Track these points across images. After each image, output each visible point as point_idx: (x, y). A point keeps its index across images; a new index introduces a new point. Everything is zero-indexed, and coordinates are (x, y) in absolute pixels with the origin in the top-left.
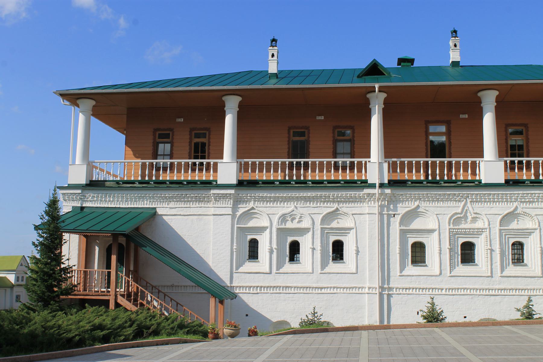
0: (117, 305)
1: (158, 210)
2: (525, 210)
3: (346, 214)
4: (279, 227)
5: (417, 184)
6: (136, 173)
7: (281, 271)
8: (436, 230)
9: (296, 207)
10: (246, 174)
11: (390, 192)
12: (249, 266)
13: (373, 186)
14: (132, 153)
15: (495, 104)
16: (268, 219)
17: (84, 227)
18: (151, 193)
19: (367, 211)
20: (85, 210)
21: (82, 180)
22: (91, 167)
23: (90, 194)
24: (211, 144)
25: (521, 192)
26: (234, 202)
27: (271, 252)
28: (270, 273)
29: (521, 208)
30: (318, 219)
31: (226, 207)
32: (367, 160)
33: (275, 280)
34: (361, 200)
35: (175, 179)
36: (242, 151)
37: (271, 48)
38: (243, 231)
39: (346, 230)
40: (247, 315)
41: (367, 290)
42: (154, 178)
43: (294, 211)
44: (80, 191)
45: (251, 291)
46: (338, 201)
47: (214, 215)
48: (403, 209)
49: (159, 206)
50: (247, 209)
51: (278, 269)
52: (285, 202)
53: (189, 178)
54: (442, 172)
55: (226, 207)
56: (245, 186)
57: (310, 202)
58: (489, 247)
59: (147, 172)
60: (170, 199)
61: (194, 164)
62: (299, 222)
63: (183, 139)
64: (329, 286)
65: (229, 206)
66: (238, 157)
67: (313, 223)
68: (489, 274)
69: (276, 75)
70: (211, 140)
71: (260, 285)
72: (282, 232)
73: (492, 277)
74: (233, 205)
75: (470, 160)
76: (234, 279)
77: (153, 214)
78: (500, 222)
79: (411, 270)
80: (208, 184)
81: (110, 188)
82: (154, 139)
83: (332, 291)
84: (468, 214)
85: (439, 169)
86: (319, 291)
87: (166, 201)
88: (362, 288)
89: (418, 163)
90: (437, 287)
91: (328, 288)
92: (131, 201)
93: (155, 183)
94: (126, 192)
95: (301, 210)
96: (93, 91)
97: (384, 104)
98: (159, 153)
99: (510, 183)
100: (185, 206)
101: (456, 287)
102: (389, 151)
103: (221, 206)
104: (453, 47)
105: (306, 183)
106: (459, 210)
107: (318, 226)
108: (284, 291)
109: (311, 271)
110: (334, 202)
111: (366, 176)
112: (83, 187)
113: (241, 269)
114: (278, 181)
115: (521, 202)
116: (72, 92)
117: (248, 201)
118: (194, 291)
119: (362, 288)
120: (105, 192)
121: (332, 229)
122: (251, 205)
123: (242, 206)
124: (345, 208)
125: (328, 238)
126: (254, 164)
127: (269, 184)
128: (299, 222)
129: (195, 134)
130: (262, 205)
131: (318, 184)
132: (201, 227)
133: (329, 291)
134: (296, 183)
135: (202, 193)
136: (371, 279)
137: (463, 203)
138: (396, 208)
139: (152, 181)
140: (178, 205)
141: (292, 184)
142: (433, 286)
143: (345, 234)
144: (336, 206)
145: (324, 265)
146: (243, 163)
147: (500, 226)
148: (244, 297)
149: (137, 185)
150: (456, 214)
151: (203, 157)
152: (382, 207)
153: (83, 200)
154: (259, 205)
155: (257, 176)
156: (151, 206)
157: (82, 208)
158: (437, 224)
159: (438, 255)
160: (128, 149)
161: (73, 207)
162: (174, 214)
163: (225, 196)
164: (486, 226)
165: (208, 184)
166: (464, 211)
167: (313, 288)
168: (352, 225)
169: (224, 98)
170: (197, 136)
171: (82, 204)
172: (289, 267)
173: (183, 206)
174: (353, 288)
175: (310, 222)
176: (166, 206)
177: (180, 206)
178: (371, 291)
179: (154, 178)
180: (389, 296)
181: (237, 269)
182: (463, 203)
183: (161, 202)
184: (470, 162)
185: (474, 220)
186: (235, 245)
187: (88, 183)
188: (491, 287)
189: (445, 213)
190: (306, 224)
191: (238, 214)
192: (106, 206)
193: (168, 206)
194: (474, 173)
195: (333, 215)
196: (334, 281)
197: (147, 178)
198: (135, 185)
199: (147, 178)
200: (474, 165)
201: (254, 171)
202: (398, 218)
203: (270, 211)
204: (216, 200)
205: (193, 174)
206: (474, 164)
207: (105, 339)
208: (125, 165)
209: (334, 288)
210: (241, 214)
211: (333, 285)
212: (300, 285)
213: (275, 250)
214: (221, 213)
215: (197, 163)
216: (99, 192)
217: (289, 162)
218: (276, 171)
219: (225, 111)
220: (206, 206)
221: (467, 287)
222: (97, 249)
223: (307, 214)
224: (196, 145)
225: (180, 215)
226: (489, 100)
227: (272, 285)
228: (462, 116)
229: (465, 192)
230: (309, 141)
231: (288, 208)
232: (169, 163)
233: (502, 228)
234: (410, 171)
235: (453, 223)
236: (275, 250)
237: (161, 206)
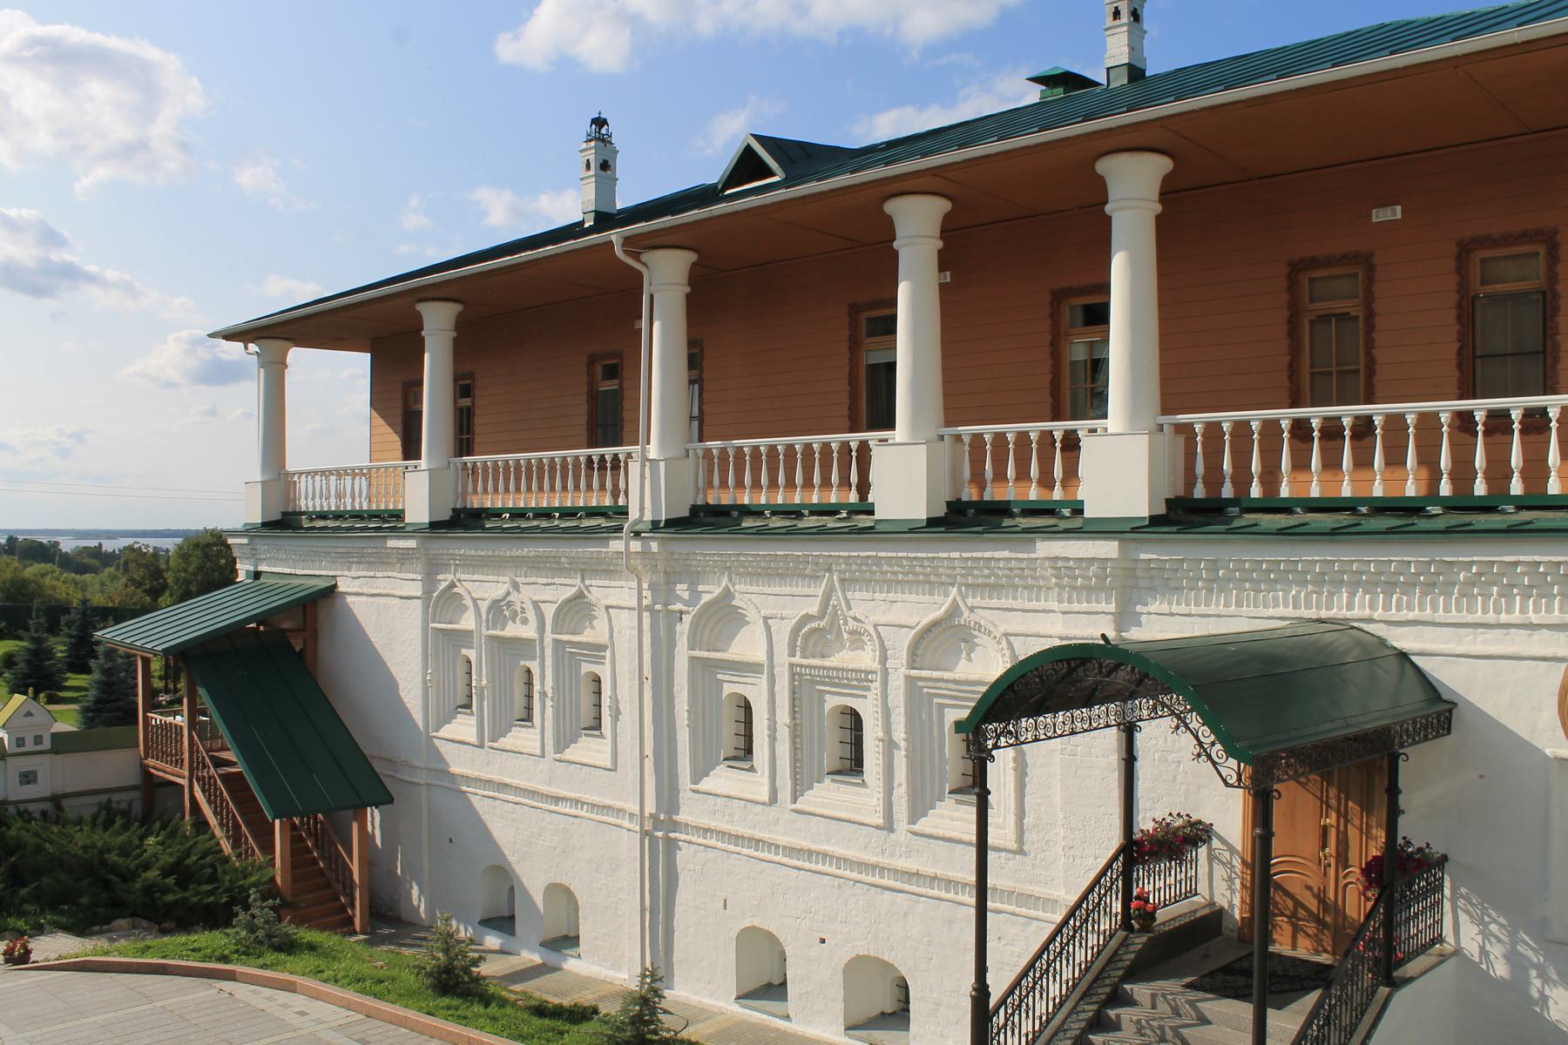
9: (516, 586)
11: (1115, 555)
15: (1158, 208)
20: (262, 580)
24: (1378, 321)
25: (956, 555)
30: (900, 644)
35: (780, 501)
42: (1445, 489)
44: (245, 541)
63: (1416, 306)
65: (1103, 606)
67: (884, 659)
70: (1378, 307)
73: (614, 769)
89: (1428, 422)
106: (814, 609)
147: (912, 665)
150: (808, 618)
169: (1105, 166)
187: (941, 511)
188: (884, 861)
189: (785, 613)
197: (1480, 488)
199: (1480, 488)
218: (1395, 459)
230: (1556, 297)
233: (914, 673)
235: (804, 649)
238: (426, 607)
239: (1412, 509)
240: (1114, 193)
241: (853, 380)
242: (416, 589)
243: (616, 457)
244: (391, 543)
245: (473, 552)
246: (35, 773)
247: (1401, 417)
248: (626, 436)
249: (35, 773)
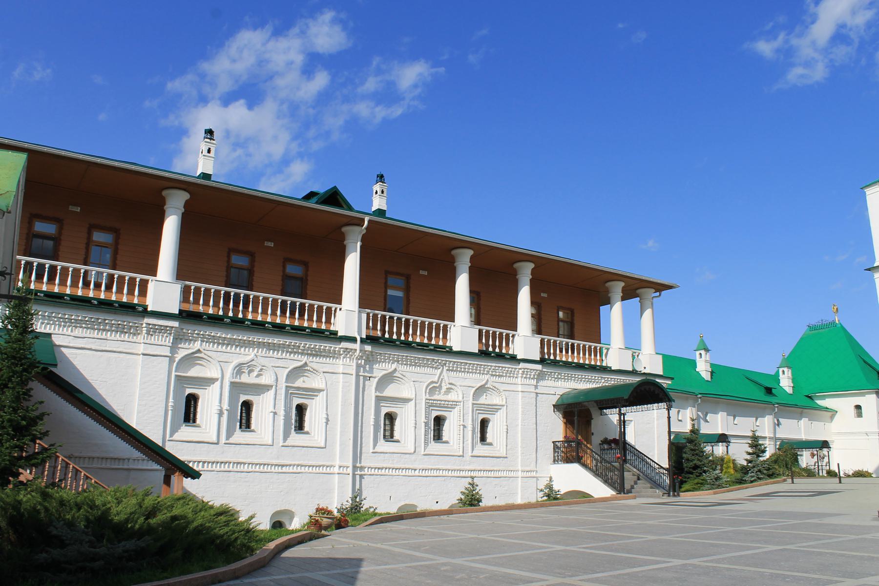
1: (54, 338)
2: (495, 384)
3: (315, 371)
5: (215, 320)
8: (217, 379)
13: (353, 340)
19: (341, 370)
26: (175, 339)
29: (492, 381)
32: (338, 306)
34: (335, 355)
39: (313, 392)
41: (336, 470)
42: (231, 314)
46: (308, 354)
48: (381, 369)
49: (56, 331)
50: (190, 351)
52: (242, 347)
54: (391, 328)
57: (274, 350)
58: (462, 423)
60: (77, 324)
62: (258, 376)
64: (293, 463)
68: (461, 453)
71: (204, 459)
72: (236, 387)
75: (325, 305)
78: (287, 375)
79: (384, 446)
80: (128, 309)
83: (295, 470)
84: (443, 384)
85: (60, 279)
86: (280, 470)
87: (69, 326)
88: (331, 466)
90: (411, 467)
91: (290, 465)
97: (184, 207)
99: (484, 354)
100: (99, 336)
101: (430, 467)
102: (182, 272)
103: (156, 342)
104: (205, 152)
107: (282, 384)
109: (270, 442)
110: (302, 354)
115: (492, 375)
118: (103, 466)
119: (331, 466)
121: (298, 388)
122: (197, 345)
124: (314, 363)
125: (291, 400)
128: (258, 376)
131: (259, 326)
133: (291, 470)
136: (341, 456)
137: (439, 371)
138: (371, 369)
140: (88, 333)
142: (407, 466)
143: (311, 397)
144: (305, 359)
145: (286, 436)
150: (433, 382)
152: (358, 366)
158: (414, 393)
159: (217, 416)
162: (80, 346)
163: (162, 330)
164: (460, 399)
166: (440, 380)
167: (272, 465)
168: (322, 386)
172: (239, 436)
173: (95, 335)
174: (320, 466)
175: (273, 378)
176: (69, 333)
178: (341, 471)
180: (361, 476)
181: (171, 436)
182: (439, 371)
183: (60, 326)
184: (138, 280)
185: (449, 390)
186: (171, 400)
188: (462, 468)
190: (266, 379)
193: (72, 334)
194: (328, 321)
195: (298, 372)
196: (297, 457)
200: (144, 285)
202: (374, 382)
204: (148, 333)
206: (445, 327)
209: (298, 466)
210: (180, 360)
211: (297, 463)
212: (256, 461)
217: (141, 280)
221: (440, 467)
223: (270, 364)
225: (90, 349)
226: (525, 272)
227: (220, 460)
228: (421, 272)
229: (102, 316)
231: (248, 355)
234: (51, 279)
236: (226, 413)
237: (60, 332)
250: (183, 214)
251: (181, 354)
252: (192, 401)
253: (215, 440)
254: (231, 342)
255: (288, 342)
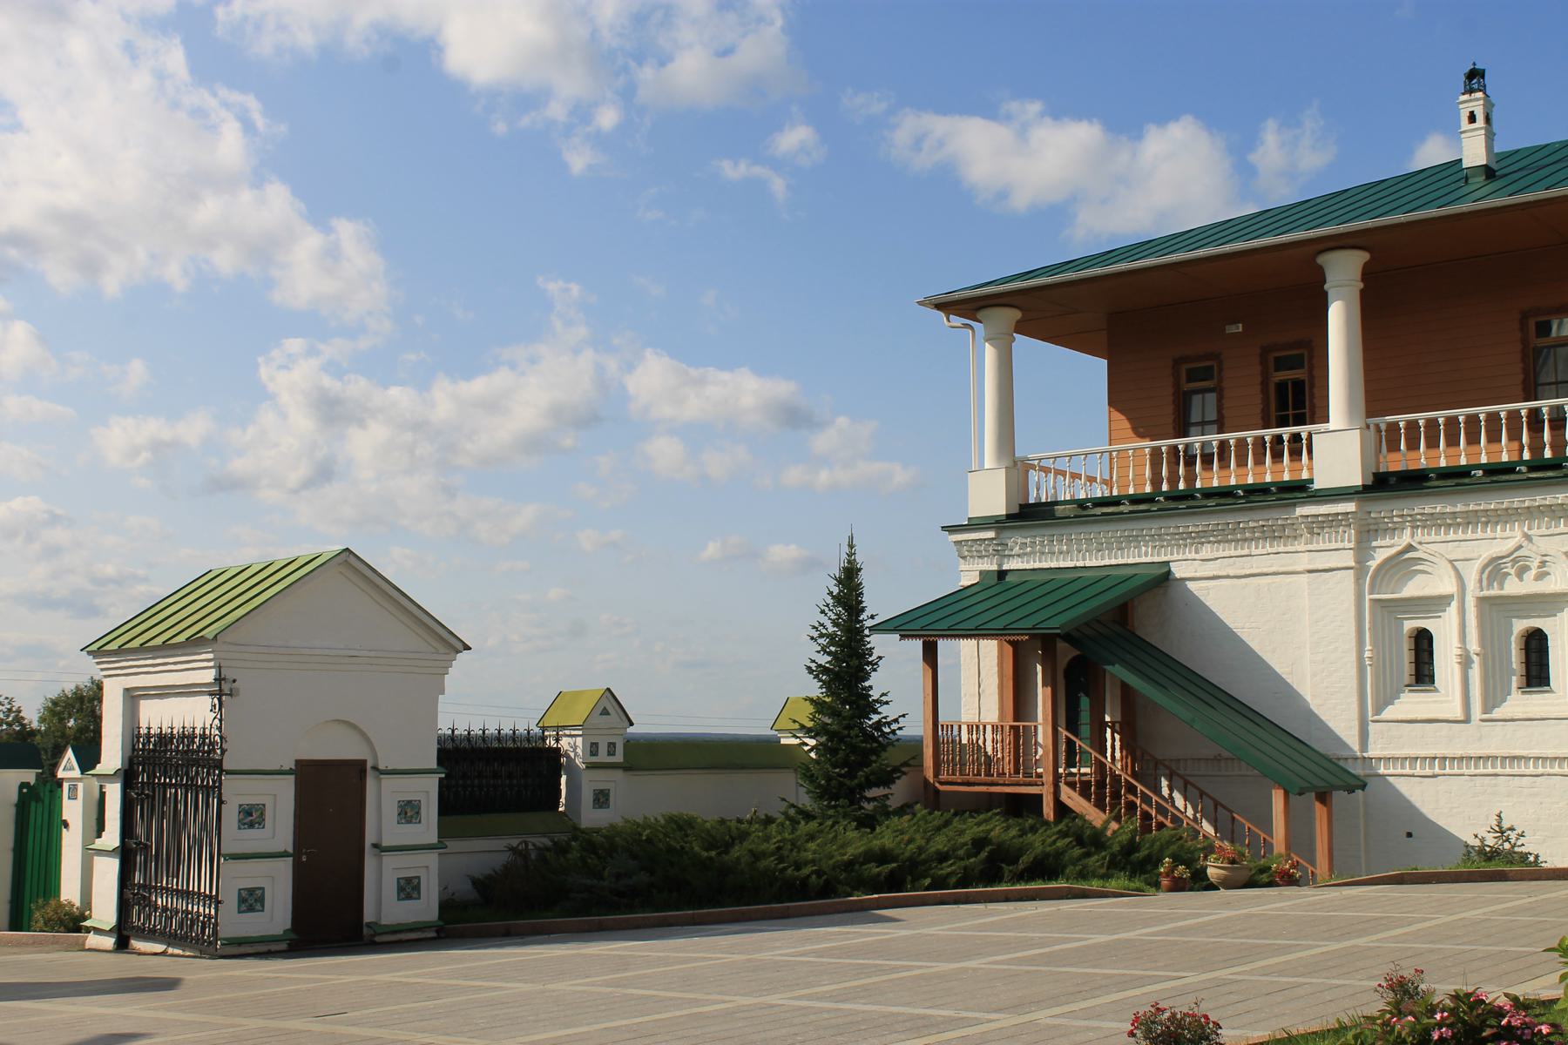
0: (1062, 809)
1: (1174, 568)
4: (1486, 593)
6: (1139, 475)
7: (1497, 713)
9: (1528, 538)
10: (1394, 456)
12: (1412, 703)
14: (1127, 424)
15: (1361, 285)
16: (1452, 573)
17: (1000, 624)
18: (1153, 526)
20: (1008, 578)
21: (997, 505)
22: (1018, 470)
23: (1016, 540)
26: (1359, 533)
27: (1466, 663)
28: (1467, 720)
30: (1472, 574)
31: (1339, 551)
33: (1480, 739)
35: (1215, 484)
36: (1378, 395)
37: (1466, 97)
38: (1391, 609)
40: (1409, 835)
42: (1526, 456)
43: (1520, 547)
44: (991, 534)
45: (1418, 771)
47: (1310, 571)
49: (1175, 557)
51: (1487, 709)
53: (1250, 480)
55: (1339, 551)
56: (1392, 488)
59: (1164, 473)
60: (1200, 538)
61: (1278, 440)
62: (1540, 576)
63: (1244, 381)
66: (1370, 413)
69: (1489, 172)
72: (1495, 609)
74: (1359, 542)
76: (1371, 740)
77: (1161, 580)
81: (1066, 521)
82: (1177, 385)
92: (1111, 550)
93: (1167, 498)
94: (1096, 528)
95: (1543, 545)
96: (1002, 288)
97: (1363, 280)
98: (1193, 420)
105: (1193, 497)
108: (1508, 770)
111: (1310, 469)
112: (1357, 493)
113: (1389, 713)
114: (1479, 466)
116: (956, 296)
117: (1393, 530)
120: (1049, 531)
122: (1405, 538)
123: (1383, 543)
126: (1412, 426)
127: (1456, 478)
129: (1277, 359)
130: (1433, 537)
132: (1282, 608)
134: (1532, 469)
135: (1277, 517)
139: (1162, 493)
141: (1520, 472)
146: (1383, 427)
148: (1403, 786)
149: (1126, 508)
151: (1300, 421)
153: (1001, 554)
154: (1427, 538)
155: (1422, 459)
156: (1156, 559)
157: (1002, 574)
159: (1457, 669)
160: (1117, 415)
161: (981, 572)
163: (1332, 521)
165: (1298, 490)
169: (1321, 260)
170: (1281, 364)
171: (1000, 565)
172: (1520, 703)
173: (1233, 553)
176: (1193, 555)
177: (1226, 553)
179: (1165, 487)
181: (1378, 711)
186: (1368, 647)
187: (1016, 510)
191: (1373, 564)
192: (1054, 564)
197: (1548, 454)
198: (1122, 508)
199: (1548, 454)
201: (1413, 445)
203: (1457, 552)
205: (1278, 466)
207: (894, 882)
208: (1111, 459)
212: (1550, 753)
213: (1475, 658)
214: (1326, 566)
215: (1286, 437)
216: (1035, 532)
219: (1325, 294)
220: (1289, 548)
222: (1039, 668)
224: (1281, 386)
225: (1228, 577)
231: (1503, 540)
232: (1215, 443)
238: (1359, 579)
239: (1508, 469)
240: (1329, 278)
241: (1265, 391)
242: (1348, 559)
243: (1296, 438)
244: (1301, 511)
245: (1460, 508)
246: (261, 809)
247: (1476, 416)
248: (1313, 414)
249: (261, 809)
250: (1362, 292)
251: (1380, 556)
252: (1423, 642)
253: (1459, 715)
254: (1470, 520)
255: (1460, 508)
